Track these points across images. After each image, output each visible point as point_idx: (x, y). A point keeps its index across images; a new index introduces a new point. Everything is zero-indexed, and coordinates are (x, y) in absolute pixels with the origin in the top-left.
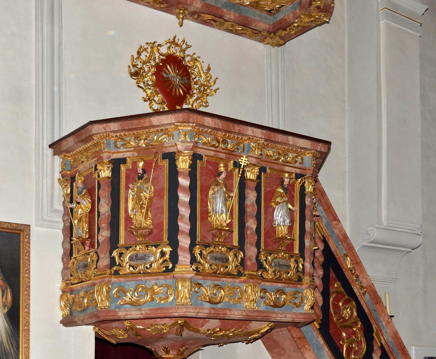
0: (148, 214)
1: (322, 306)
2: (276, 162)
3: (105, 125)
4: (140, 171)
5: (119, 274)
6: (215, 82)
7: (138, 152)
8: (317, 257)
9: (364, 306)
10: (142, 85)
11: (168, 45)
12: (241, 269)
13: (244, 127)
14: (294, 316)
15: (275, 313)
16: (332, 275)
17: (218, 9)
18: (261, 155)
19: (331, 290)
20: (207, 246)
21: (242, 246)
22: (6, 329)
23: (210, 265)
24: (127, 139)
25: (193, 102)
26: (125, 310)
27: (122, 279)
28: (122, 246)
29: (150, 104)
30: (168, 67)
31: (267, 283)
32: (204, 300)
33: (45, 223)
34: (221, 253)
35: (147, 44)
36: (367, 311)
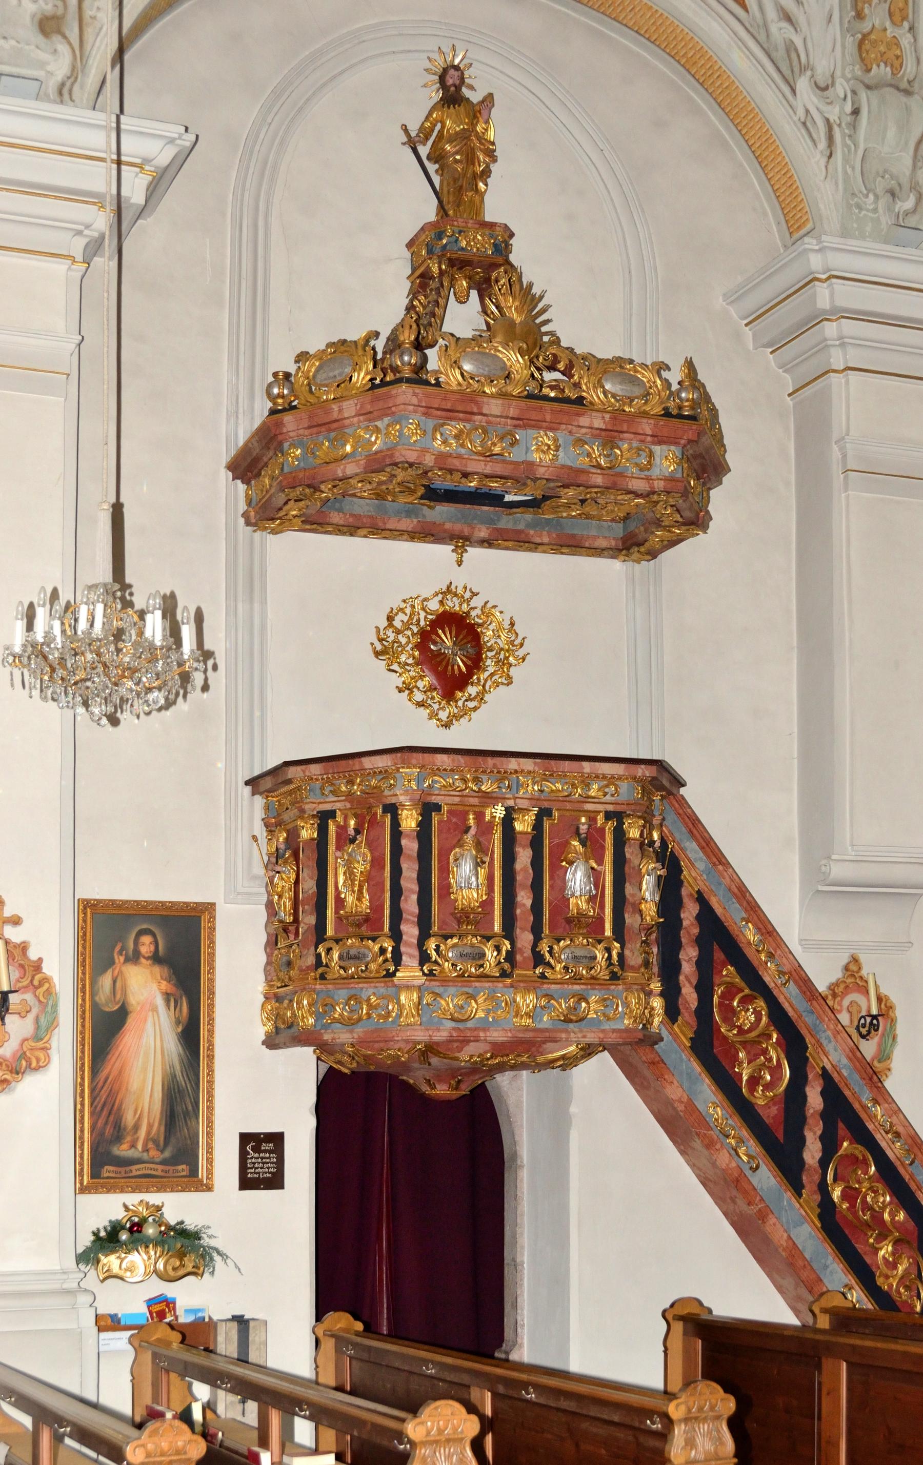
0: (362, 893)
1: (696, 1009)
2: (567, 799)
3: (303, 767)
4: (351, 832)
5: (325, 979)
6: (522, 645)
7: (351, 802)
8: (686, 928)
9: (786, 1006)
10: (395, 667)
11: (440, 597)
12: (507, 966)
13: (504, 759)
14: (601, 1035)
15: (566, 1031)
16: (718, 955)
17: (520, 532)
18: (541, 791)
19: (716, 980)
20: (446, 937)
21: (509, 930)
22: (179, 1055)
23: (453, 965)
24: (338, 782)
25: (486, 681)
26: (333, 1032)
27: (330, 987)
28: (331, 938)
29: (409, 695)
30: (440, 632)
31: (553, 986)
32: (442, 1016)
33: (240, 897)
34: (472, 946)
35: (404, 601)
36: (791, 1013)
